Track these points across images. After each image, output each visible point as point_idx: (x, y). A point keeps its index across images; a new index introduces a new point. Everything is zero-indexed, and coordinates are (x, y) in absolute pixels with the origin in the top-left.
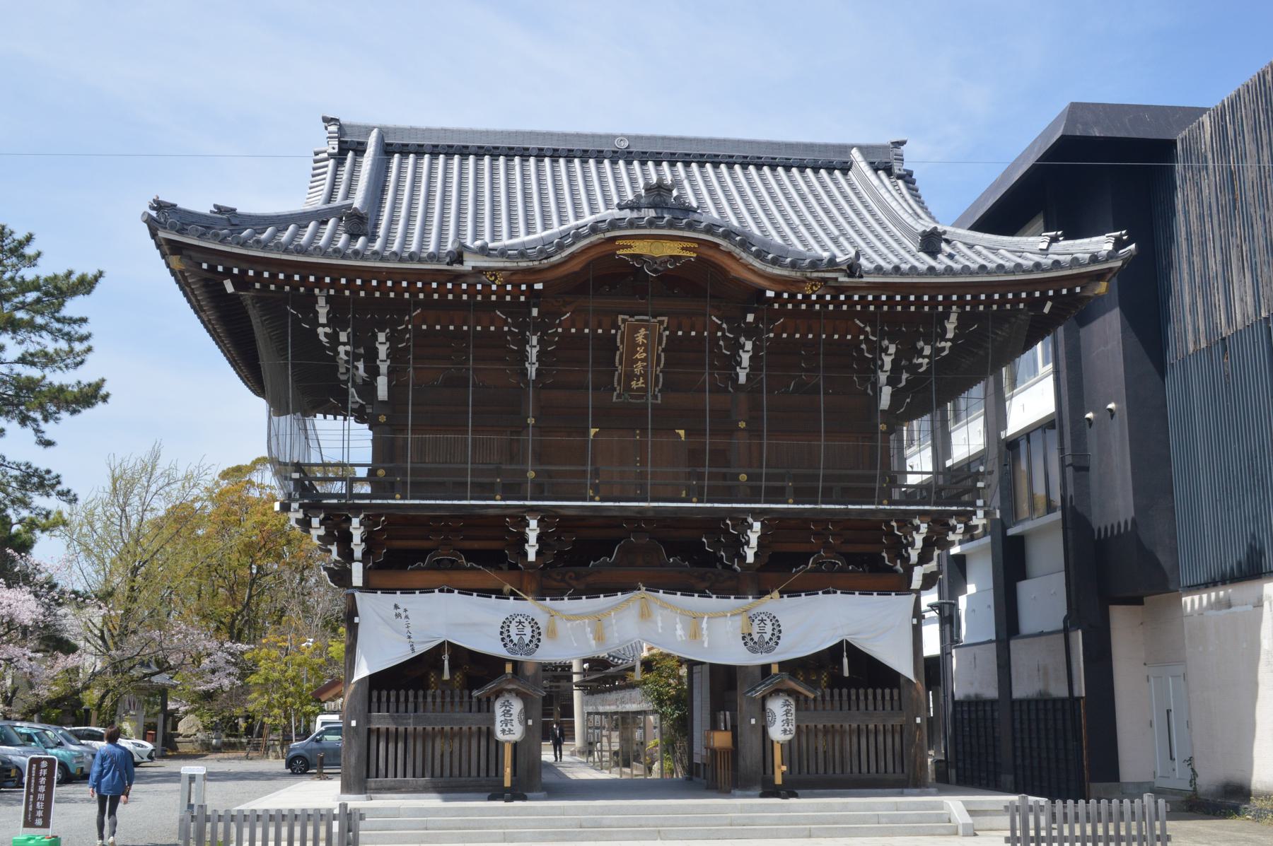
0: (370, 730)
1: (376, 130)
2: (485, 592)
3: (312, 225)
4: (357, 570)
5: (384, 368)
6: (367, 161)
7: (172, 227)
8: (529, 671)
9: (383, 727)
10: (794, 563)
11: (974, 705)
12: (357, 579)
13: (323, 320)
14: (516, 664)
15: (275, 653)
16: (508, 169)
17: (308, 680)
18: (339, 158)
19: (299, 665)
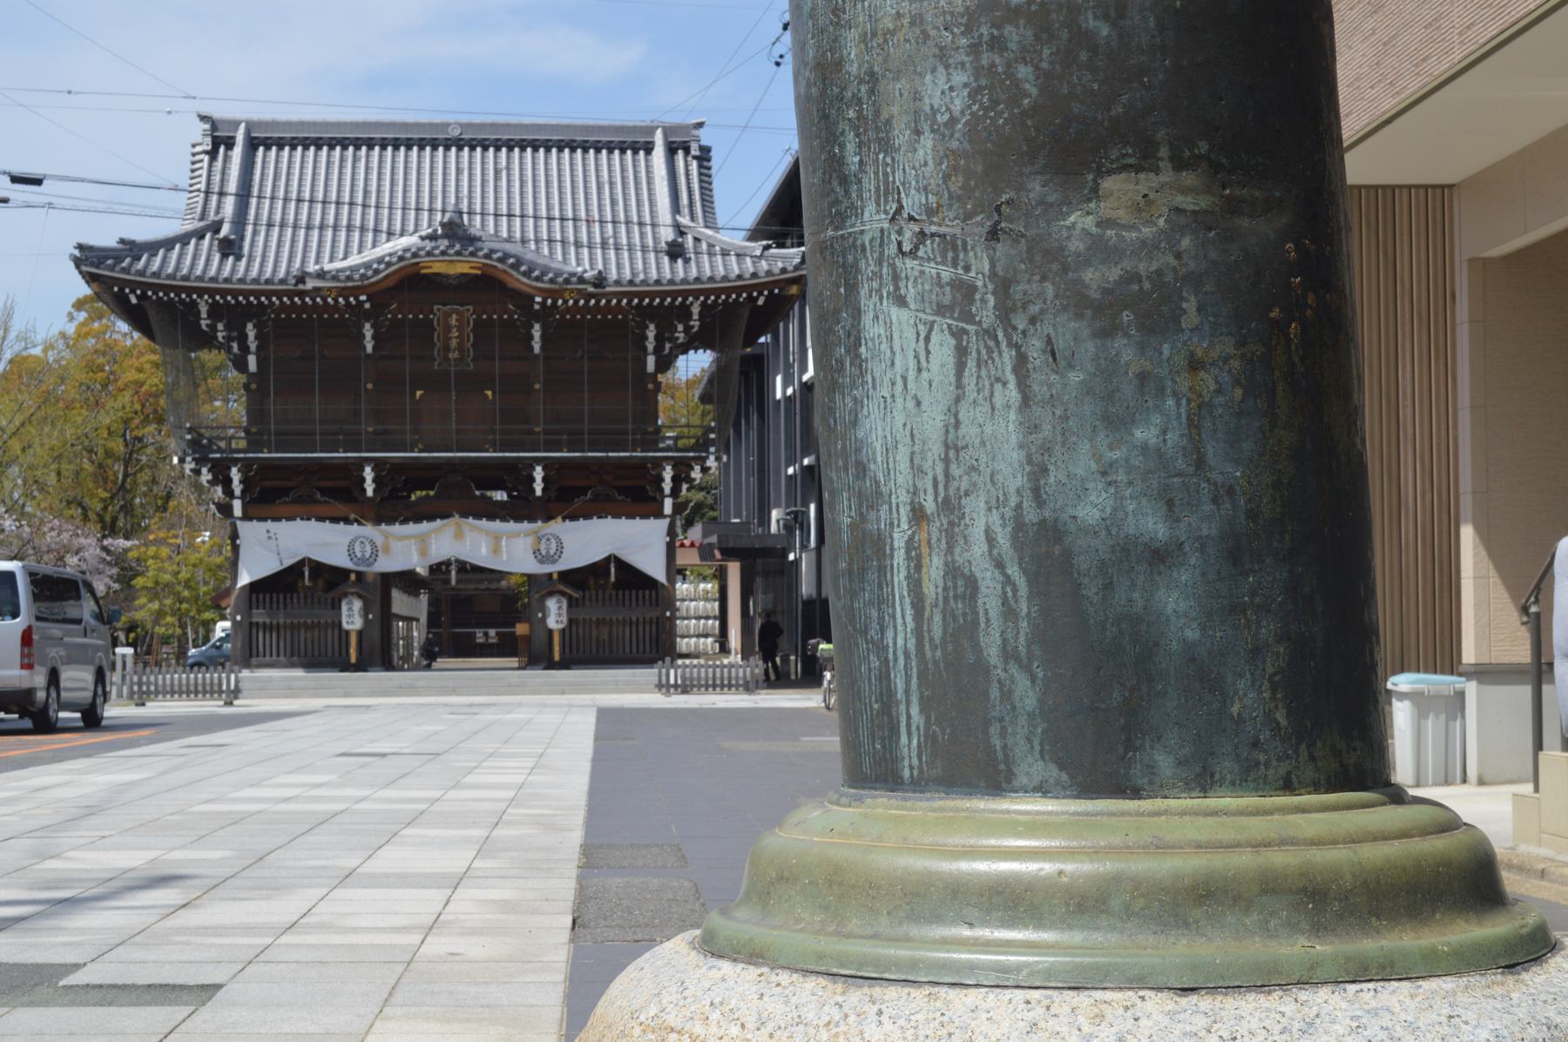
0: (251, 624)
1: (243, 125)
2: (335, 520)
3: (193, 241)
4: (237, 507)
5: (253, 346)
6: (237, 152)
7: (92, 265)
8: (370, 579)
9: (261, 620)
10: (574, 495)
13: (204, 315)
14: (359, 574)
16: (355, 160)
17: (206, 583)
18: (213, 154)
19: (194, 566)
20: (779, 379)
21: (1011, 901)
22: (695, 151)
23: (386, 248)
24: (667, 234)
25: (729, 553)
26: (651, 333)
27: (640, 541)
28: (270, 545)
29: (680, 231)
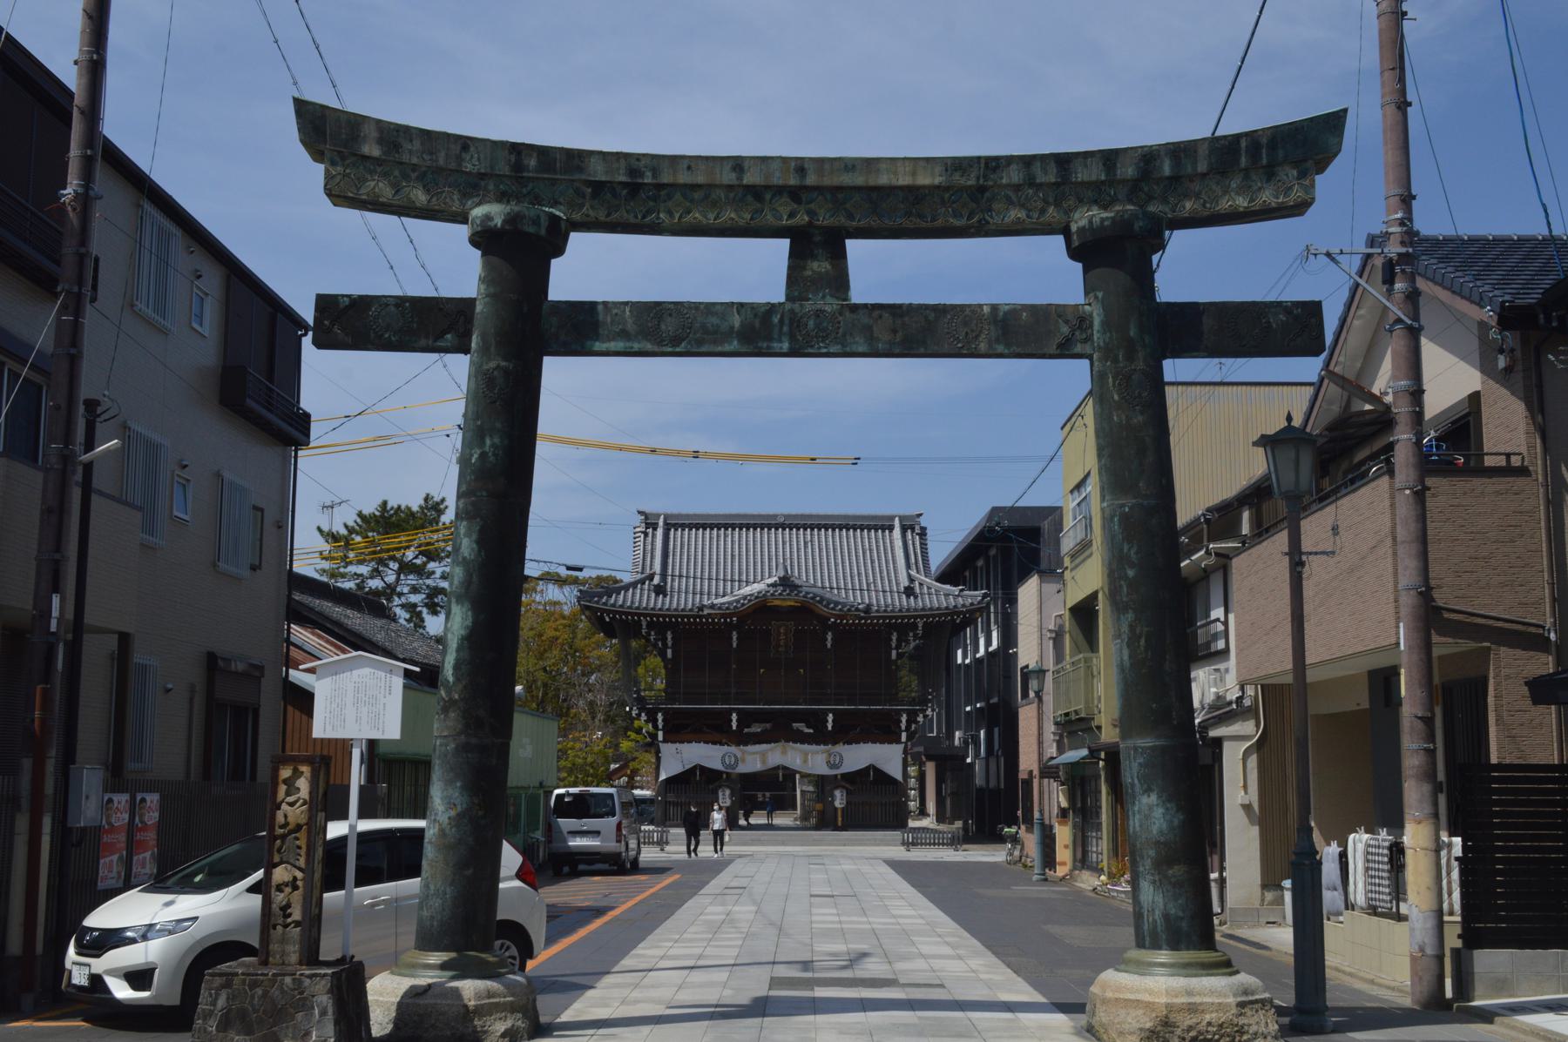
2: (714, 743)
4: (660, 735)
6: (660, 532)
10: (850, 730)
11: (980, 790)
12: (660, 737)
15: (578, 745)
20: (960, 652)
21: (1162, 965)
22: (917, 530)
23: (747, 590)
24: (904, 582)
25: (930, 758)
26: (894, 638)
27: (888, 757)
28: (677, 758)
29: (911, 580)
